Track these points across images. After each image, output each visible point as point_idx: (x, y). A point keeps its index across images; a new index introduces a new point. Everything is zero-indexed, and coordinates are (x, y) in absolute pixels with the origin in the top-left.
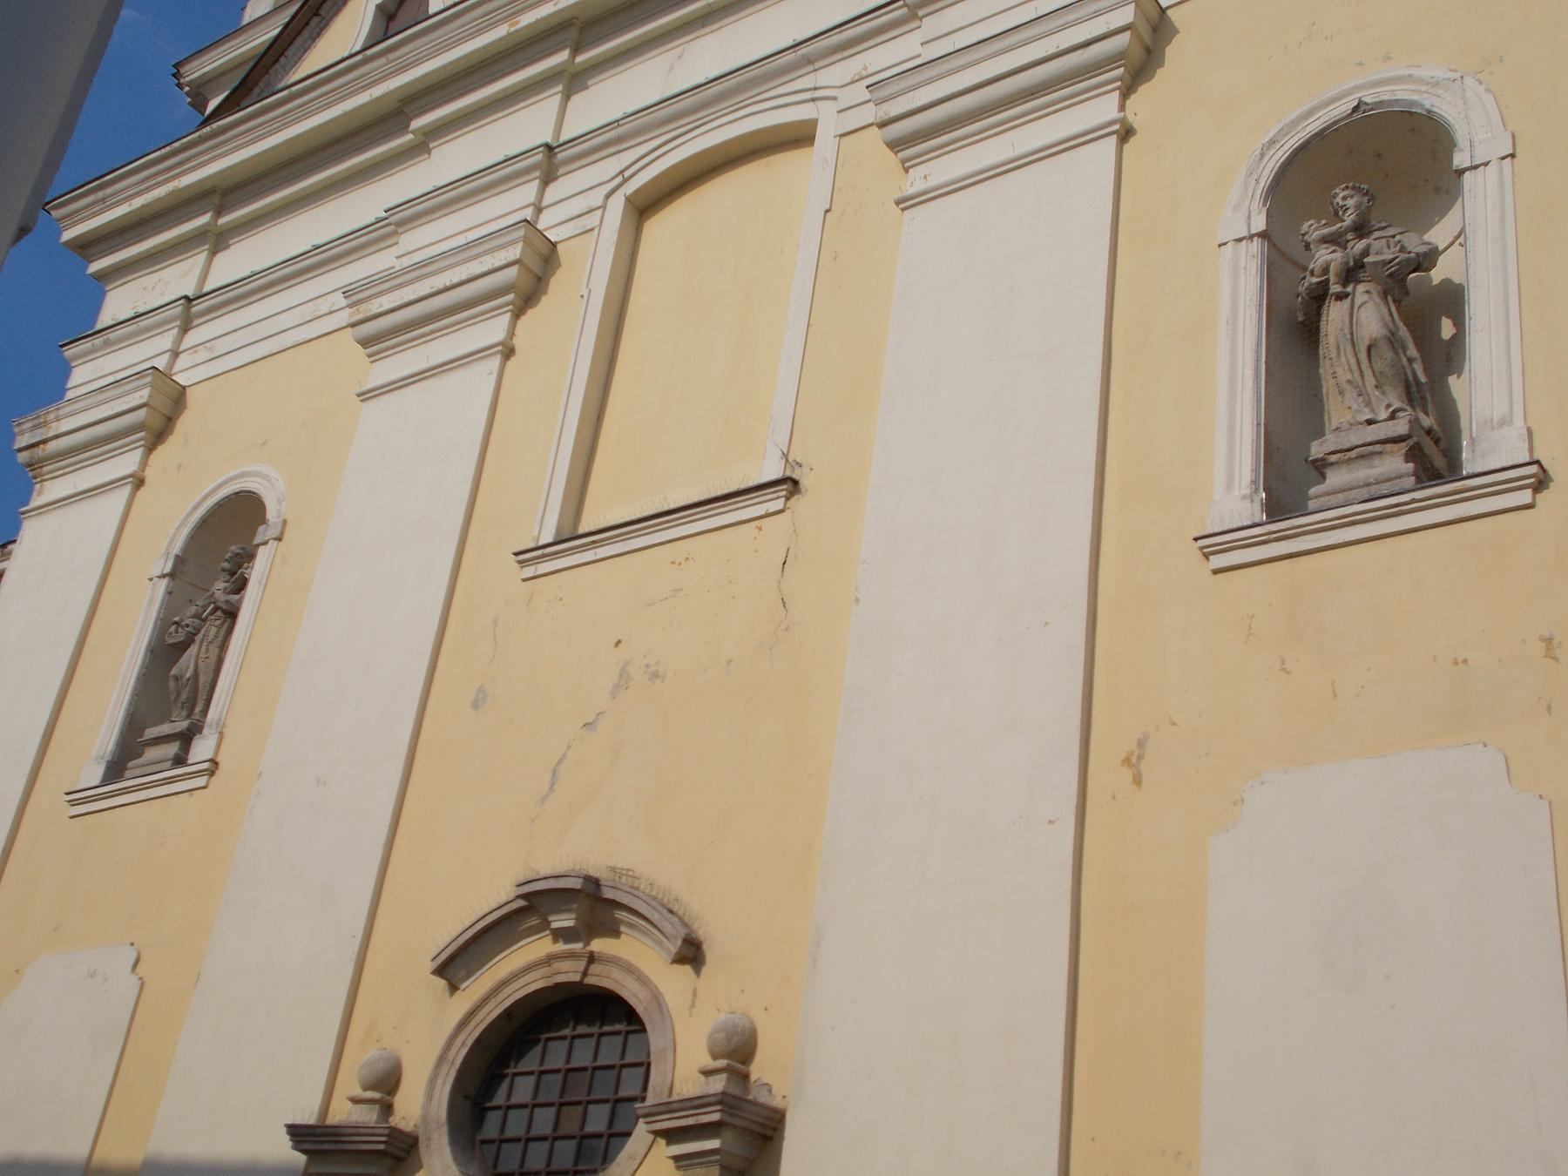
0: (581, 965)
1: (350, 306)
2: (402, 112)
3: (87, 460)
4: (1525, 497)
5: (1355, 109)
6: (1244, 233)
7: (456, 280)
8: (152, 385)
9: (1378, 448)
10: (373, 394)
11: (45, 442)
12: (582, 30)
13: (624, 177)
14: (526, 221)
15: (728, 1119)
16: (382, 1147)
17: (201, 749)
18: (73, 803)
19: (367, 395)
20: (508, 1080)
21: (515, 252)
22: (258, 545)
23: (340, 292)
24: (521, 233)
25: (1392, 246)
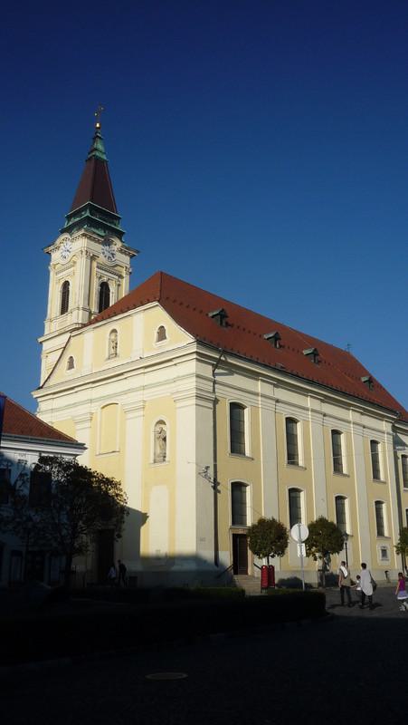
17: (167, 459)
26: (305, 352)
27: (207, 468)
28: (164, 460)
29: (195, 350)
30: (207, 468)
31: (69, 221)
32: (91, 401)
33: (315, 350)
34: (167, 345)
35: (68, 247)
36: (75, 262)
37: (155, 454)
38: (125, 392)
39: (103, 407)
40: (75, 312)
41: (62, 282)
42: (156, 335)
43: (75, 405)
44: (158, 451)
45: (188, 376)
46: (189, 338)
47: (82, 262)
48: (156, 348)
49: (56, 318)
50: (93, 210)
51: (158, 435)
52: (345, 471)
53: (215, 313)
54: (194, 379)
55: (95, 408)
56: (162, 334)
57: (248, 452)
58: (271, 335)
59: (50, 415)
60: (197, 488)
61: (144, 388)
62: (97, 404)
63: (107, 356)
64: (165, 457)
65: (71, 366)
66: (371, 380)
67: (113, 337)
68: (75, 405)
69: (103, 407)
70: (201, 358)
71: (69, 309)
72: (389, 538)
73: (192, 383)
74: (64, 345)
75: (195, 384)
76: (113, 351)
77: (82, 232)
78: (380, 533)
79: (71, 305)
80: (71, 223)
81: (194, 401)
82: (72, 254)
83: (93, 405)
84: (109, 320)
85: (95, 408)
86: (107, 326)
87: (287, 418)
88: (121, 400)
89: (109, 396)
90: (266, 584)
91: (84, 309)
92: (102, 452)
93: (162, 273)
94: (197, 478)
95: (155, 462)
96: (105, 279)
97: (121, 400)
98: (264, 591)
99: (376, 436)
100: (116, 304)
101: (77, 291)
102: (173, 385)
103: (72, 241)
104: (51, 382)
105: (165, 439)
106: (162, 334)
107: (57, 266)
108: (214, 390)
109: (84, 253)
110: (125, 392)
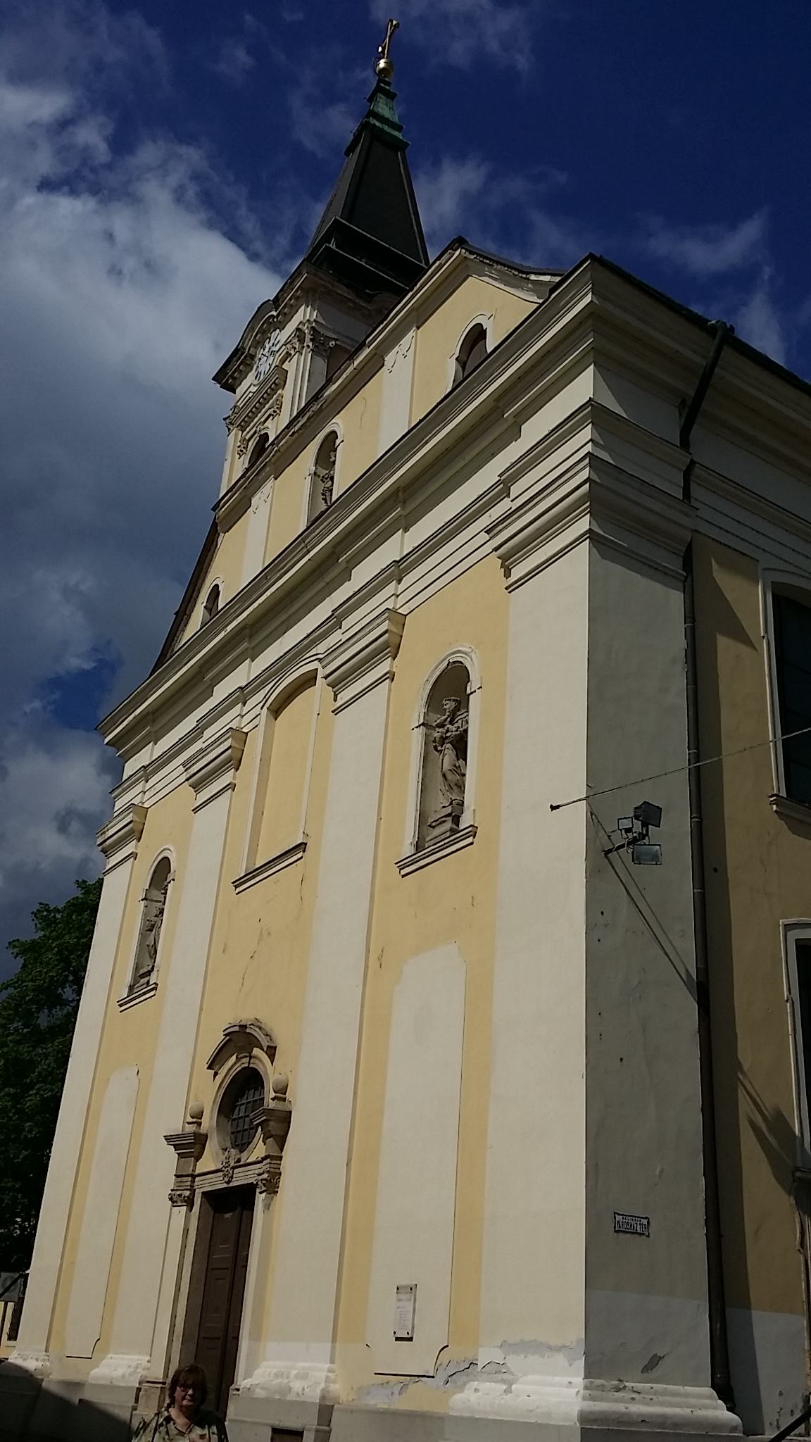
0: (248, 1059)
1: (185, 771)
2: (201, 672)
3: (351, 680)
4: (470, 840)
5: (448, 665)
6: (417, 725)
7: (212, 758)
8: (590, 464)
9: (444, 819)
10: (381, 680)
11: (105, 841)
12: (404, 492)
13: (266, 699)
14: (387, 609)
15: (269, 1118)
16: (193, 1141)
17: (465, 821)
18: (120, 1006)
19: (195, 810)
20: (238, 1108)
21: (585, 474)
22: (469, 695)
23: (181, 766)
24: (587, 461)
25: (460, 721)
30: (649, 815)
37: (422, 816)
94: (592, 874)
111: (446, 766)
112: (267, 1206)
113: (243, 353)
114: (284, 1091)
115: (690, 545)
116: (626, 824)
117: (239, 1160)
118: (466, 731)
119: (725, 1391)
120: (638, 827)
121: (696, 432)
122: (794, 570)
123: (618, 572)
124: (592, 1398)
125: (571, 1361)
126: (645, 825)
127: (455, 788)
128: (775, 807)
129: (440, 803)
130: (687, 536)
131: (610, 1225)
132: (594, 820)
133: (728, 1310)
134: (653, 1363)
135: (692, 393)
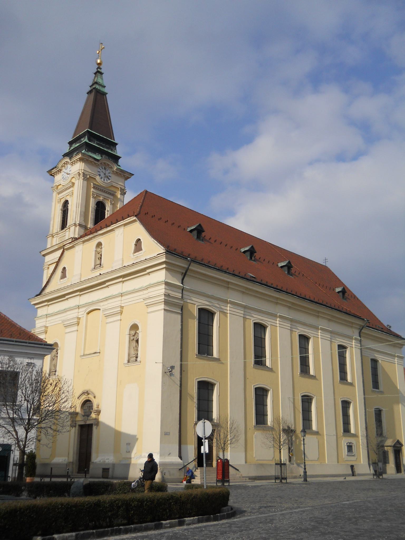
17: (138, 359)
26: (280, 265)
27: (172, 367)
28: (136, 360)
29: (164, 260)
30: (172, 367)
31: (71, 147)
32: (79, 307)
33: (289, 262)
34: (142, 255)
35: (68, 171)
36: (73, 184)
37: (129, 355)
38: (106, 299)
39: (88, 313)
40: (72, 228)
41: (63, 201)
42: (133, 247)
43: (65, 311)
44: (133, 352)
45: (164, 283)
46: (161, 249)
47: (79, 183)
48: (131, 258)
49: (57, 233)
50: (91, 136)
51: (132, 338)
52: (312, 372)
53: (193, 228)
54: (163, 286)
55: (82, 313)
56: (138, 245)
57: (215, 354)
58: (247, 249)
59: (44, 320)
60: (162, 386)
61: (122, 295)
62: (84, 309)
63: (93, 266)
64: (137, 357)
65: (64, 275)
66: (344, 292)
67: (99, 250)
68: (65, 311)
69: (88, 313)
70: (170, 268)
71: (68, 224)
72: (355, 436)
73: (161, 290)
74: (57, 260)
75: (163, 290)
76: (98, 262)
77: (80, 156)
78: (347, 430)
79: (70, 221)
80: (72, 148)
81: (162, 306)
82: (70, 177)
83: (81, 310)
84: (95, 234)
85: (82, 313)
86: (93, 240)
87: (255, 324)
88: (101, 306)
89: (93, 303)
90: (220, 477)
91: (80, 225)
92: (87, 352)
93: (146, 192)
94: (163, 376)
95: (129, 362)
96: (101, 199)
97: (101, 306)
98: (150, 459)
99: (344, 342)
100: (108, 218)
101: (74, 209)
102: (145, 292)
103: (72, 164)
104: (48, 290)
105: (137, 341)
106: (138, 245)
107: (59, 187)
108: (182, 297)
109: (82, 174)
110: (106, 299)
111: (134, 346)
112: (96, 428)
113: (58, 168)
114: (98, 406)
115: (182, 306)
116: (169, 368)
117: (87, 419)
118: (138, 339)
119: (180, 457)
120: (171, 369)
121: (184, 292)
122: (203, 304)
123: (169, 314)
124: (160, 459)
125: (158, 454)
126: (172, 369)
127: (136, 351)
128: (195, 356)
129: (98, 262)
130: (182, 305)
131: (164, 434)
132: (163, 366)
133: (181, 446)
134: (170, 454)
135: (185, 272)
